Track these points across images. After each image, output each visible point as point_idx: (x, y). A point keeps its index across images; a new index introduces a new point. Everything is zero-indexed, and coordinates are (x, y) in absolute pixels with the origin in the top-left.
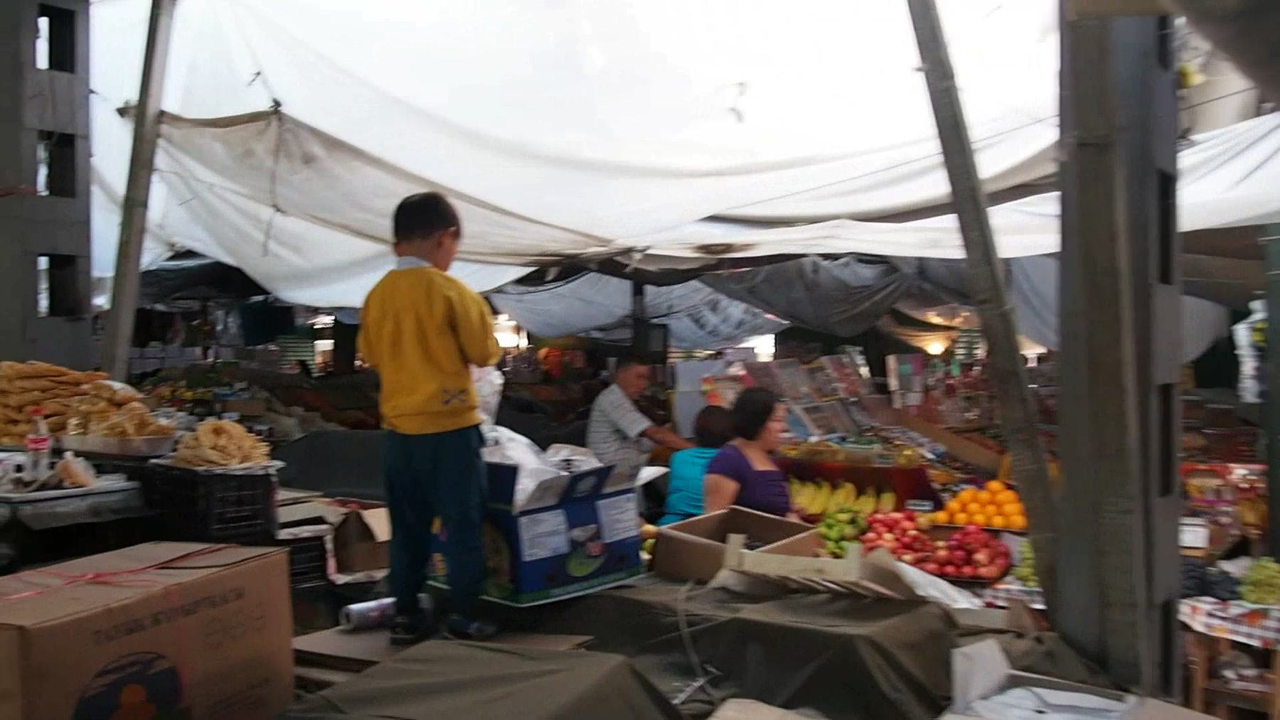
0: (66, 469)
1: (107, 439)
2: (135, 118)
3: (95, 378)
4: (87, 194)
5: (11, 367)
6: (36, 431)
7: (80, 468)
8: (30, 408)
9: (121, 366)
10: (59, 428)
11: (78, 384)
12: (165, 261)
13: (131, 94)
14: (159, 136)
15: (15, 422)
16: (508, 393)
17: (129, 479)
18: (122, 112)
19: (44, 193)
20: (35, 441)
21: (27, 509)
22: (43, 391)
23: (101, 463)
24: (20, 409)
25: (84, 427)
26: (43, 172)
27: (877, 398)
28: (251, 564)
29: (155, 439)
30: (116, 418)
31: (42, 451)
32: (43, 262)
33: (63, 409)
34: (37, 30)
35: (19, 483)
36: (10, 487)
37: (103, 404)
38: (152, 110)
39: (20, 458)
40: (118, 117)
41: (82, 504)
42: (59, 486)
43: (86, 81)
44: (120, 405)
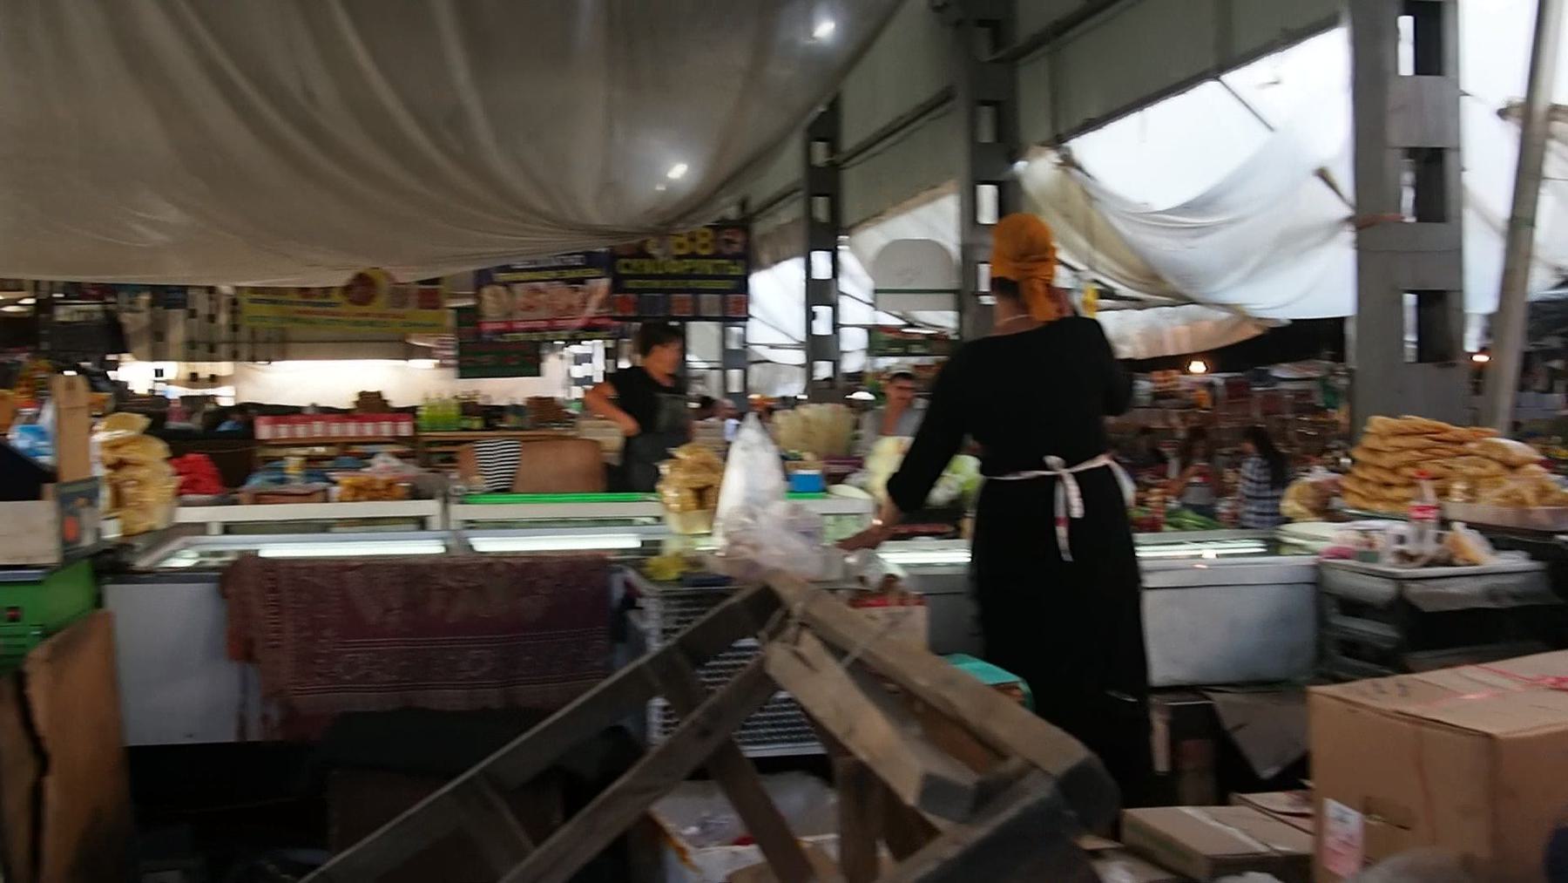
0: (1456, 543)
1: (1499, 508)
2: (1520, 121)
3: (1483, 435)
4: (1460, 218)
5: (1383, 422)
6: (1421, 497)
7: (1474, 545)
8: (1410, 472)
9: (1504, 417)
10: (1443, 493)
11: (1461, 443)
12: (1545, 290)
13: (1516, 90)
14: (1551, 136)
15: (1388, 485)
16: (246, 359)
17: (1533, 558)
18: (1503, 113)
19: (1411, 219)
20: (1421, 509)
21: (1415, 588)
22: (1420, 450)
23: (1499, 538)
24: (1394, 470)
25: (1472, 494)
26: (1408, 196)
27: (216, 576)
28: (1443, 732)
29: (1559, 510)
30: (1511, 484)
31: (1428, 520)
32: (1410, 300)
33: (1442, 470)
34: (1397, 31)
35: (1405, 557)
36: (1392, 560)
37: (1494, 467)
38: (1541, 105)
39: (1400, 527)
40: (1497, 121)
41: (1476, 586)
42: (1449, 563)
43: (1456, 83)
44: (1512, 467)
